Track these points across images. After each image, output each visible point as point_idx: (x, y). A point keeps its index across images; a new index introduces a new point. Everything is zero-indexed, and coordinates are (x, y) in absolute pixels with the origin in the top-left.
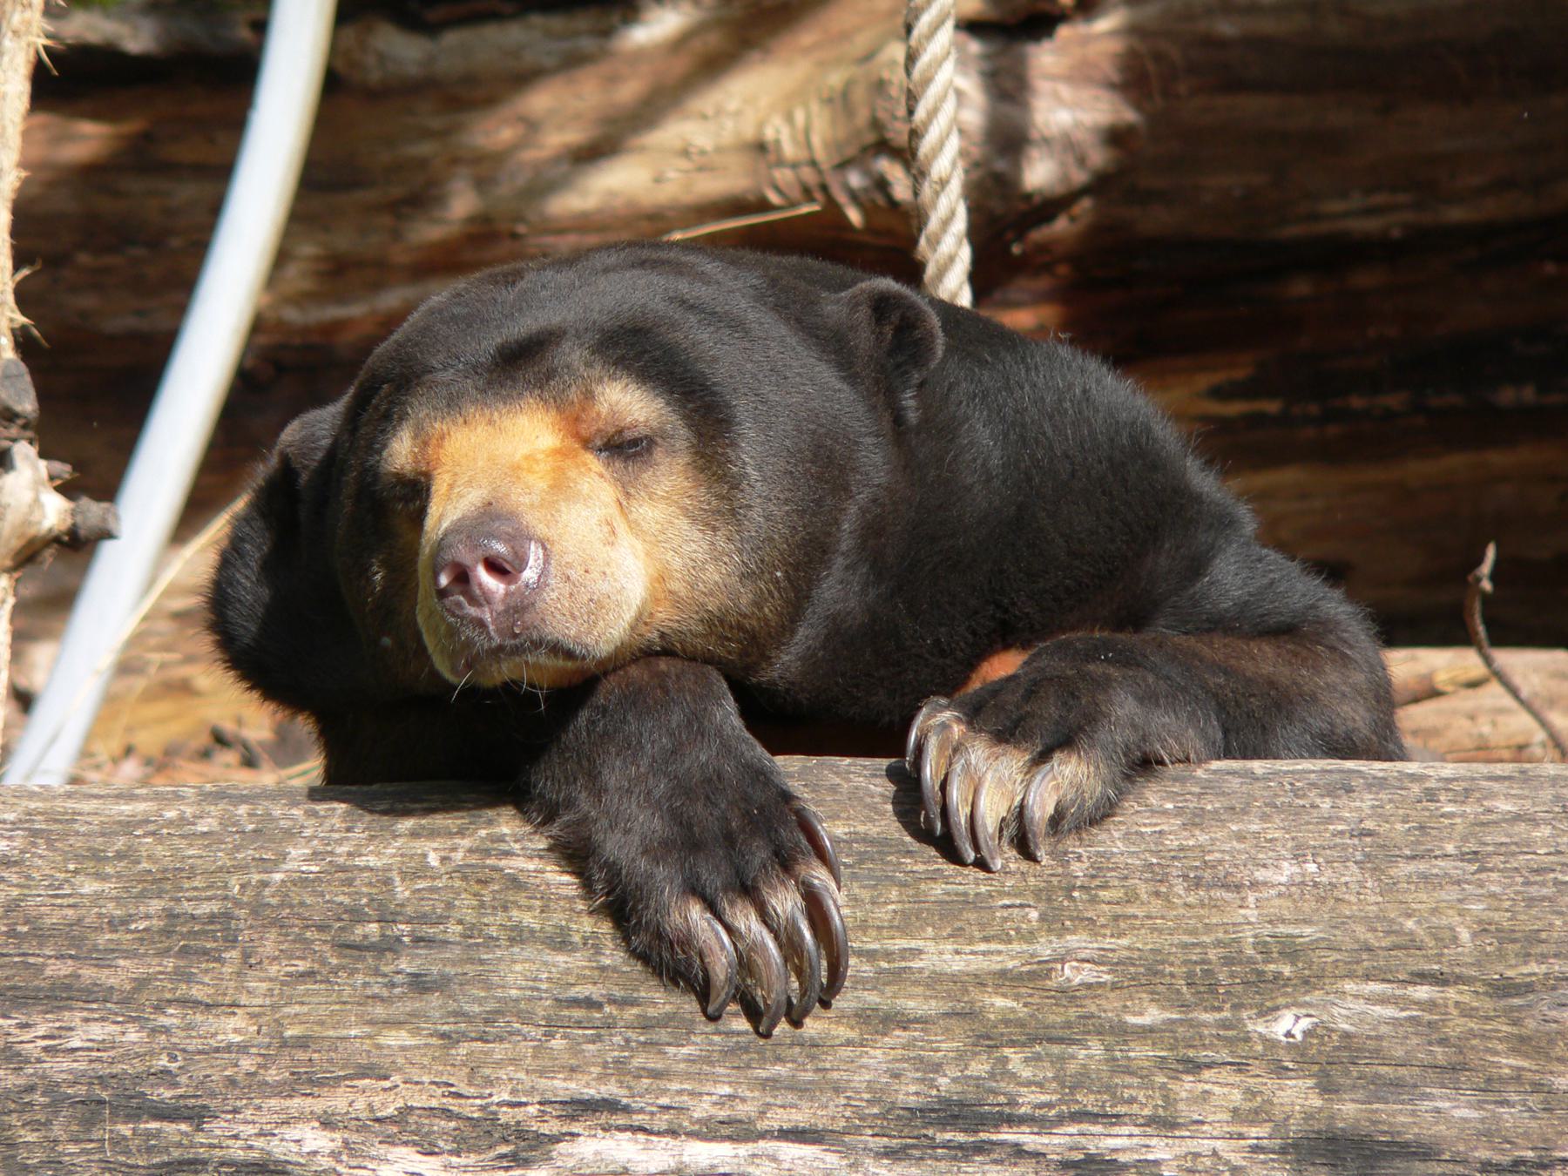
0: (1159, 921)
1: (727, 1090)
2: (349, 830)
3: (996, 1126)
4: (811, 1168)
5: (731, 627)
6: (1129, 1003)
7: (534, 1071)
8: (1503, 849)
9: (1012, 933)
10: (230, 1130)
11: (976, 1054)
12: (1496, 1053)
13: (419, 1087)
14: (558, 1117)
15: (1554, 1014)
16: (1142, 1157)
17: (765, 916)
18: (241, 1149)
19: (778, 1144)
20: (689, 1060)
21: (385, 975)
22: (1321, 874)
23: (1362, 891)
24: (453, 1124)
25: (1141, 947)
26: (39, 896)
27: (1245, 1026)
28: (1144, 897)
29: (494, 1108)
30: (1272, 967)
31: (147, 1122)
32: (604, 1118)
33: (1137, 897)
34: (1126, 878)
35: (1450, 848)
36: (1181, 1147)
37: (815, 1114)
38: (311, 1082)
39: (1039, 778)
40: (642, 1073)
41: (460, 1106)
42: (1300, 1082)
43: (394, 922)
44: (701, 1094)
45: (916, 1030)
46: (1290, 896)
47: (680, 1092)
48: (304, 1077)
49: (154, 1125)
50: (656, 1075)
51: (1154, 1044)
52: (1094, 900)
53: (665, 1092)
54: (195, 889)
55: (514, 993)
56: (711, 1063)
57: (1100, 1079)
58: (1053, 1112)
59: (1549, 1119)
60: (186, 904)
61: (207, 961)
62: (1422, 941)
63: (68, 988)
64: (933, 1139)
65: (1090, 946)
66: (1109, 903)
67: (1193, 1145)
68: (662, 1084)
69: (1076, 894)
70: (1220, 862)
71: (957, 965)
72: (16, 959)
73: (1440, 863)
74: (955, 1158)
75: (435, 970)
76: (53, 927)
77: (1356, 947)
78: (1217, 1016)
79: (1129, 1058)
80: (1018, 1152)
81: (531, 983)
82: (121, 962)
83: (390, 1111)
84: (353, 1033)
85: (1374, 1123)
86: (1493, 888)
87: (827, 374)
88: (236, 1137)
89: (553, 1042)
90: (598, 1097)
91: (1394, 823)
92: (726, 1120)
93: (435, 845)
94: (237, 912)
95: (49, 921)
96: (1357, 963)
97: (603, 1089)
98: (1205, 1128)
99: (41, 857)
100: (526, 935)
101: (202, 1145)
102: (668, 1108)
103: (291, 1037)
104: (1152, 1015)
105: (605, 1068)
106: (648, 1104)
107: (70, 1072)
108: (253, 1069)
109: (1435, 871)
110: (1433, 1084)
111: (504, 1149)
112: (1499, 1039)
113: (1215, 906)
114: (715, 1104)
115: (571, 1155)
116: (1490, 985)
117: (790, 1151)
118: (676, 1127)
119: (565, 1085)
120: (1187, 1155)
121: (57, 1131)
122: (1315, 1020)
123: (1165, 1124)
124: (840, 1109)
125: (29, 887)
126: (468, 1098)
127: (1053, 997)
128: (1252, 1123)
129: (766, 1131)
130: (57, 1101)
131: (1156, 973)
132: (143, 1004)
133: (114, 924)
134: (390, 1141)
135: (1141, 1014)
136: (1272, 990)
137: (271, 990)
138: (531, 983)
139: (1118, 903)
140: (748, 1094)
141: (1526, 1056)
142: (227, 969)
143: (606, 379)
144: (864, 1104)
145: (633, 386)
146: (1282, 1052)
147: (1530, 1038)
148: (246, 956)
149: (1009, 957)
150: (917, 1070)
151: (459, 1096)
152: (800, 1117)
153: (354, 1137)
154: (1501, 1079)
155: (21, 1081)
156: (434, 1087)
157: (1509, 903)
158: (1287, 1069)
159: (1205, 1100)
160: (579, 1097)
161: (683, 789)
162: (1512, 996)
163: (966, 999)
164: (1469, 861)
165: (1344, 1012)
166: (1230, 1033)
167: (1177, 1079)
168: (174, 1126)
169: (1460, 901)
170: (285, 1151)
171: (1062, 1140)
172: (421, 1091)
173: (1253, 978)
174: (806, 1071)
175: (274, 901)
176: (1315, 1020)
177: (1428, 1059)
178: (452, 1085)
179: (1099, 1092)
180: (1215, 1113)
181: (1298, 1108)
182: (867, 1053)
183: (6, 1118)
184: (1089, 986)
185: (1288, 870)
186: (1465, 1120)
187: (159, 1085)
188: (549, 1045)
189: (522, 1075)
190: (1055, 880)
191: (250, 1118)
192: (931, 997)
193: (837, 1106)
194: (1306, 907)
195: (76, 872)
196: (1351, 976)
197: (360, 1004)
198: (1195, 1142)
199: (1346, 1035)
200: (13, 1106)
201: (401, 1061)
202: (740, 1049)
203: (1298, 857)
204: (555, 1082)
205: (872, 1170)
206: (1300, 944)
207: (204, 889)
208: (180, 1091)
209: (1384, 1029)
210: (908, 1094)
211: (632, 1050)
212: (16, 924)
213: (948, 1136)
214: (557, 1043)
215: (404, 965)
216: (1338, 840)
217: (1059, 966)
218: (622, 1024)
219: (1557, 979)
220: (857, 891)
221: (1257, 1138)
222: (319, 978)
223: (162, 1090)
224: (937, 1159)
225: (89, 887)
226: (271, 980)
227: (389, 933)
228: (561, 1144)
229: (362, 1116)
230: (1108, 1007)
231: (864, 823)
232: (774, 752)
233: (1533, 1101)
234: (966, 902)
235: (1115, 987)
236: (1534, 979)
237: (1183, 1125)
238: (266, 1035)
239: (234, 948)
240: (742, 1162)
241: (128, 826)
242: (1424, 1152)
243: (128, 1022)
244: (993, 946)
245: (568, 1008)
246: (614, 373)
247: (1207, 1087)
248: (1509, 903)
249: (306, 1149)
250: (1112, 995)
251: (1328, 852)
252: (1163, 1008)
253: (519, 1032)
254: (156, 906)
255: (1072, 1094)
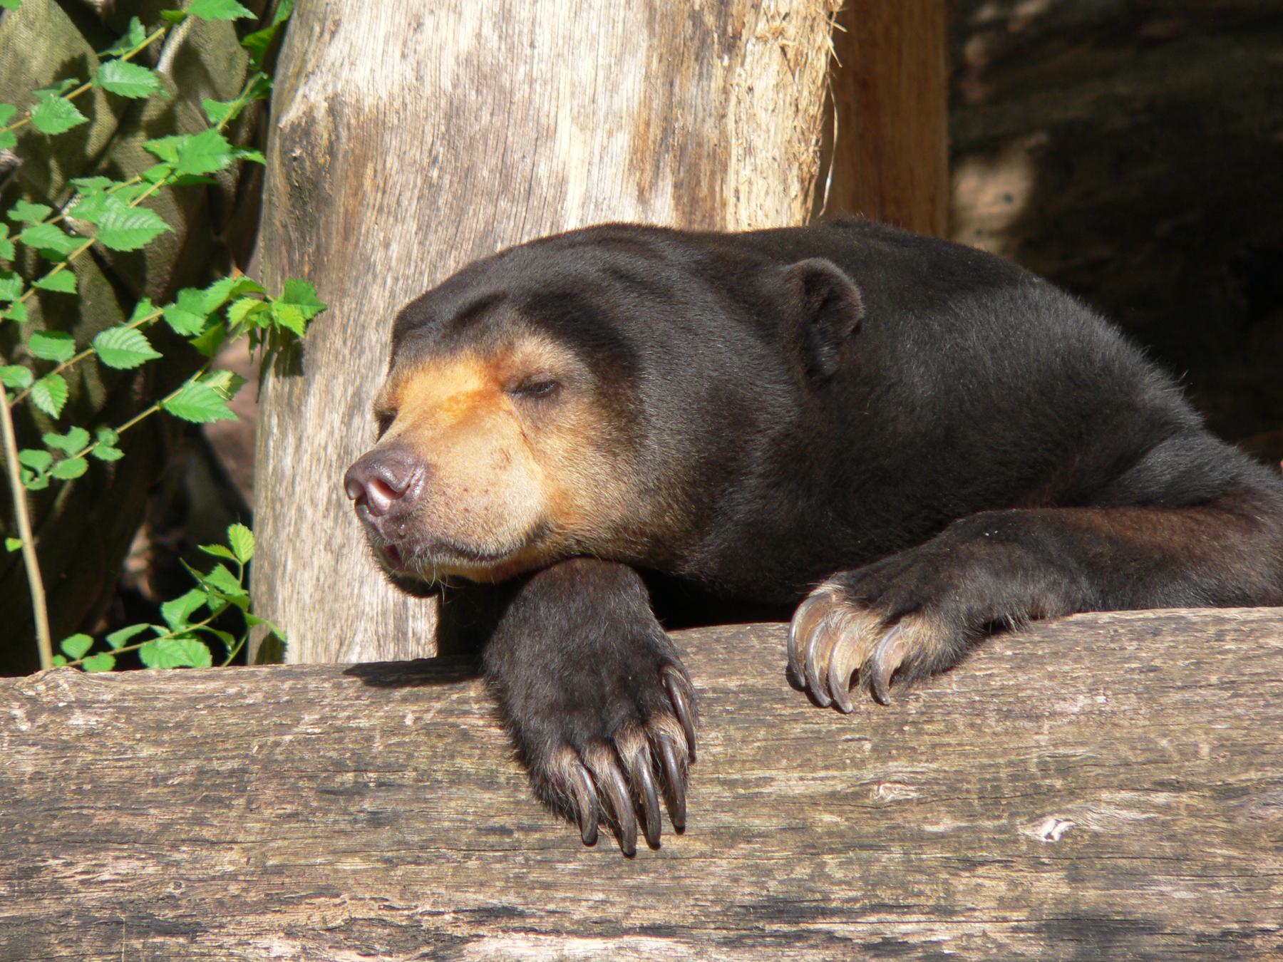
0: (967, 748)
1: (600, 896)
2: (358, 698)
3: (813, 918)
4: (666, 957)
5: (634, 532)
6: (929, 815)
7: (452, 887)
8: (1256, 678)
9: (848, 761)
10: (216, 941)
11: (800, 860)
12: (1212, 845)
13: (362, 902)
14: (469, 923)
15: (1260, 812)
16: (928, 939)
17: (619, 763)
18: (224, 956)
19: (639, 938)
20: (574, 874)
21: (351, 814)
22: (1106, 704)
23: (1135, 717)
24: (387, 931)
25: (947, 768)
26: (106, 760)
27: (1016, 830)
28: (961, 728)
29: (418, 917)
30: (1048, 782)
31: (154, 937)
32: (504, 922)
33: (955, 728)
34: (949, 713)
35: (1214, 679)
36: (958, 930)
37: (669, 913)
38: (281, 902)
39: (886, 638)
40: (535, 885)
41: (392, 916)
42: (1053, 875)
43: (366, 771)
44: (580, 900)
45: (757, 843)
46: (1078, 722)
47: (564, 900)
48: (275, 897)
49: (159, 940)
50: (547, 886)
51: (943, 847)
52: (920, 732)
53: (551, 899)
54: (226, 750)
55: (446, 824)
56: (590, 875)
57: (896, 877)
58: (858, 905)
59: (1250, 897)
60: (215, 762)
61: (219, 808)
62: (1170, 756)
63: (109, 832)
64: (763, 930)
65: (905, 770)
66: (931, 734)
67: (967, 928)
68: (551, 893)
69: (906, 728)
70: (1030, 697)
71: (798, 789)
72: (74, 811)
73: (1202, 692)
74: (780, 945)
75: (389, 808)
76: (110, 785)
77: (1118, 763)
78: (996, 823)
79: (921, 860)
80: (831, 938)
81: (460, 816)
82: (152, 811)
83: (339, 922)
84: (319, 861)
85: (1110, 905)
86: (1238, 711)
87: (742, 335)
88: (221, 947)
89: (469, 863)
90: (499, 905)
91: (1177, 660)
92: (599, 920)
93: (415, 708)
94: (251, 767)
95: (107, 780)
96: (1115, 776)
97: (504, 899)
98: (977, 914)
99: (119, 729)
100: (463, 777)
101: (196, 954)
102: (553, 912)
103: (272, 866)
104: (946, 824)
105: (507, 882)
106: (538, 910)
107: (99, 899)
108: (237, 893)
109: (1197, 698)
110: (1160, 872)
111: (426, 950)
112: (1215, 834)
113: (1017, 733)
114: (590, 908)
115: (478, 952)
116: (1214, 790)
117: (649, 944)
118: (559, 927)
119: (475, 896)
120: (962, 935)
121: (85, 947)
122: (1072, 823)
123: (945, 912)
124: (690, 909)
125: (101, 753)
126: (398, 909)
127: (869, 813)
128: (1014, 909)
129: (630, 928)
130: (87, 922)
131: (955, 790)
132: (163, 844)
133: (157, 780)
134: (337, 946)
135: (937, 823)
136: (1043, 801)
137: (263, 829)
138: (460, 816)
139: (939, 734)
140: (618, 899)
141: (1237, 847)
142: (233, 814)
143: (527, 335)
144: (708, 904)
145: (548, 341)
146: (1041, 850)
147: (1240, 833)
148: (249, 802)
149: (839, 781)
150: (752, 875)
151: (392, 908)
152: (658, 916)
153: (310, 944)
154: (1216, 867)
155: (60, 908)
156: (373, 902)
157: (1248, 722)
158: (1044, 864)
159: (977, 891)
160: (484, 906)
161: (573, 662)
162: (1230, 798)
163: (801, 816)
164: (1226, 689)
165: (1095, 816)
166: (1003, 836)
167: (957, 875)
168: (174, 939)
169: (1209, 722)
170: (257, 956)
171: (865, 927)
172: (362, 905)
173: (1030, 791)
174: (664, 879)
175: (280, 758)
176: (1072, 823)
177: (1158, 853)
178: (387, 900)
179: (895, 888)
180: (984, 901)
181: (1050, 895)
182: (714, 863)
183: (47, 938)
184: (898, 802)
185: (1083, 701)
186: (1183, 900)
187: (165, 908)
188: (466, 865)
189: (442, 890)
190: (892, 717)
191: (231, 931)
192: (774, 816)
193: (687, 906)
194: (1087, 732)
195: (140, 740)
196: (1108, 787)
197: (327, 838)
198: (969, 925)
199: (1096, 835)
200: (52, 928)
201: (351, 882)
202: (615, 863)
203: (1093, 691)
204: (467, 895)
205: (714, 956)
206: (1074, 762)
207: (232, 750)
208: (181, 912)
209: (1126, 829)
210: (743, 895)
211: (530, 867)
212: (83, 783)
213: (775, 927)
214: (473, 864)
215: (367, 805)
216: (1128, 676)
217: (876, 787)
218: (526, 846)
219: (1268, 783)
220: (732, 732)
221: (1017, 921)
222: (301, 818)
223: (167, 912)
224: (765, 946)
225: (146, 751)
226: (264, 821)
227: (360, 780)
228: (470, 944)
229: (317, 926)
230: (910, 820)
231: (754, 677)
232: (669, 626)
233: (1239, 883)
234: (818, 737)
235: (920, 802)
236: (1249, 784)
237: (960, 912)
238: (252, 865)
239: (242, 796)
240: (611, 953)
241: (193, 701)
242: (1151, 927)
243: (149, 858)
244: (831, 773)
245: (485, 835)
246: (535, 330)
247: (980, 881)
248: (1248, 722)
249: (273, 955)
250: (916, 809)
251: (1117, 686)
252: (955, 818)
253: (444, 856)
254: (192, 764)
255: (874, 890)
